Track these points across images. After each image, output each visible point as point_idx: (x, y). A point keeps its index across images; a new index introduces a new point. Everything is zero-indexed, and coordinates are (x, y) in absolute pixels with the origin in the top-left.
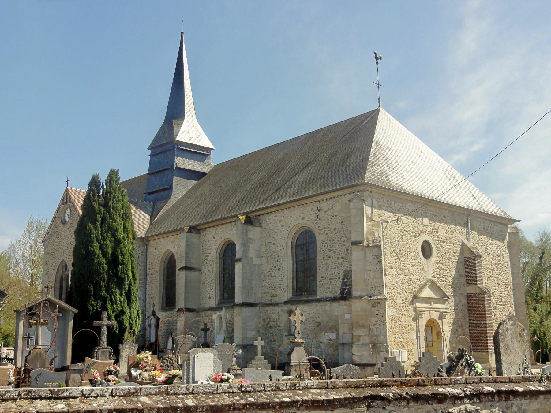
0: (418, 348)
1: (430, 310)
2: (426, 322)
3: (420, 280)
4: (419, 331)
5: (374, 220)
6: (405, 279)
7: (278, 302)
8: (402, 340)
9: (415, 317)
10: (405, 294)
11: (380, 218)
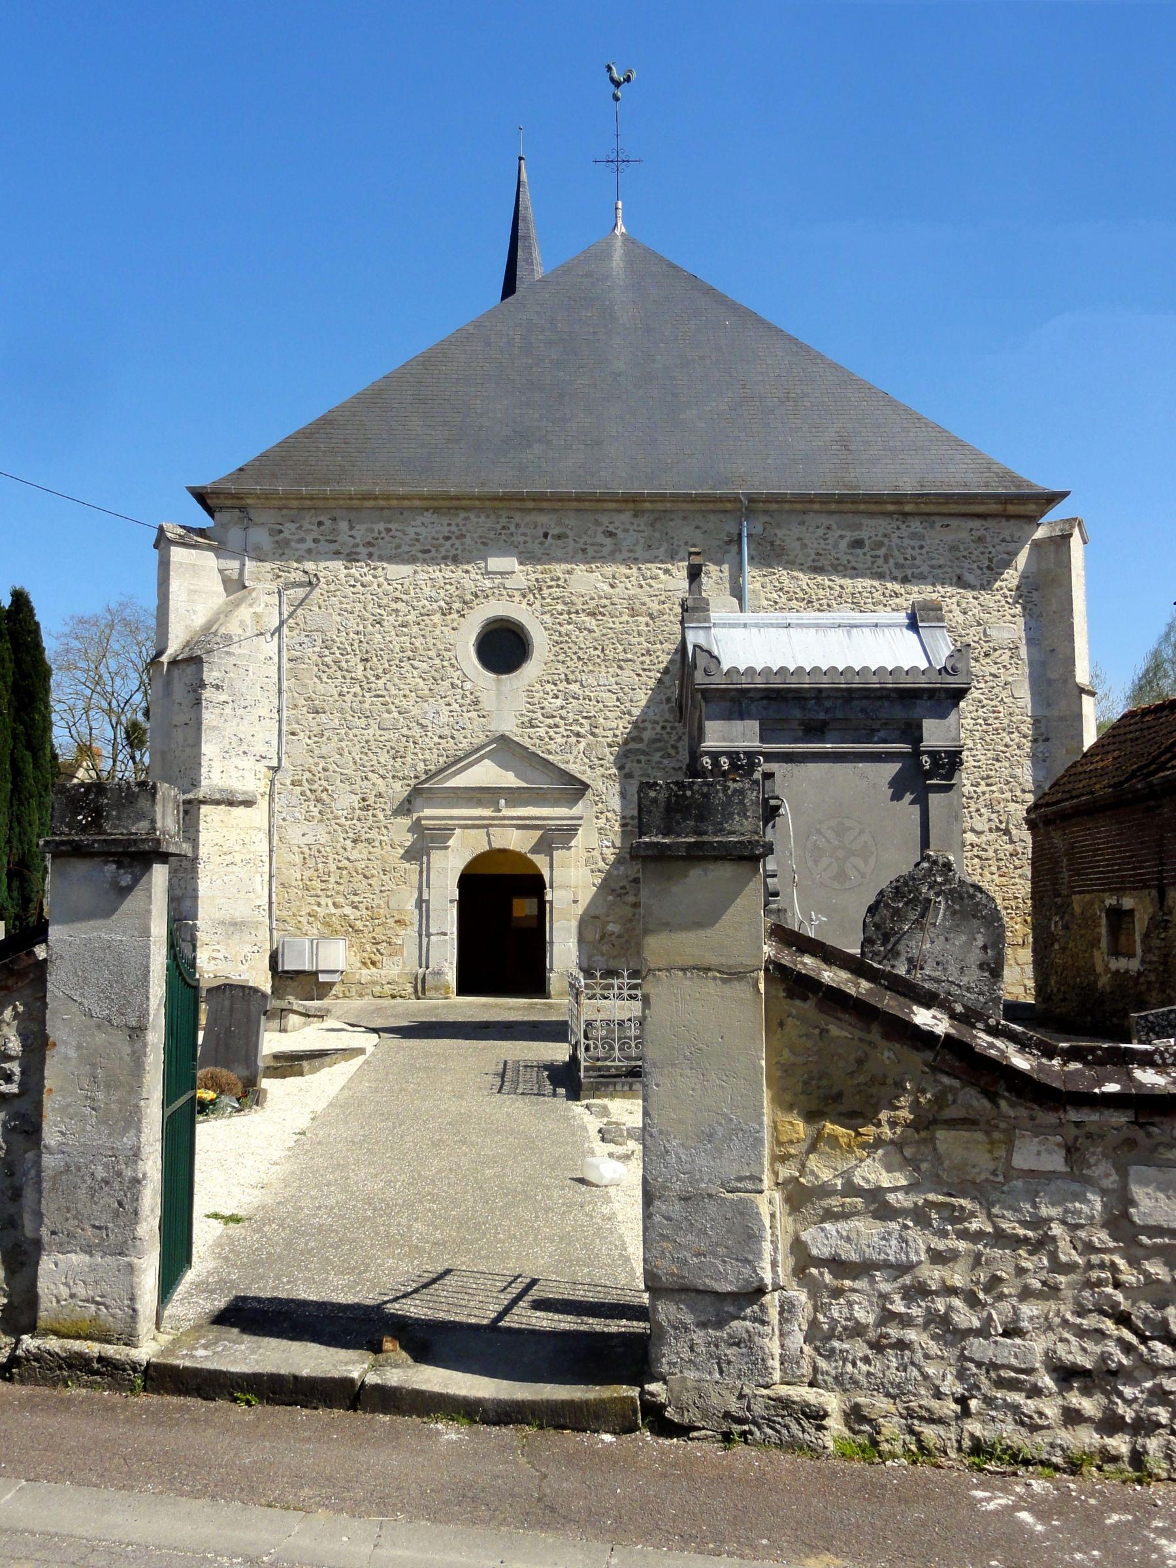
0: (420, 936)
1: (491, 826)
2: (469, 859)
3: (453, 738)
4: (428, 886)
5: (245, 587)
6: (382, 739)
7: (21, 1525)
8: (348, 910)
9: (418, 846)
10: (380, 781)
11: (280, 577)
